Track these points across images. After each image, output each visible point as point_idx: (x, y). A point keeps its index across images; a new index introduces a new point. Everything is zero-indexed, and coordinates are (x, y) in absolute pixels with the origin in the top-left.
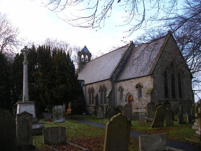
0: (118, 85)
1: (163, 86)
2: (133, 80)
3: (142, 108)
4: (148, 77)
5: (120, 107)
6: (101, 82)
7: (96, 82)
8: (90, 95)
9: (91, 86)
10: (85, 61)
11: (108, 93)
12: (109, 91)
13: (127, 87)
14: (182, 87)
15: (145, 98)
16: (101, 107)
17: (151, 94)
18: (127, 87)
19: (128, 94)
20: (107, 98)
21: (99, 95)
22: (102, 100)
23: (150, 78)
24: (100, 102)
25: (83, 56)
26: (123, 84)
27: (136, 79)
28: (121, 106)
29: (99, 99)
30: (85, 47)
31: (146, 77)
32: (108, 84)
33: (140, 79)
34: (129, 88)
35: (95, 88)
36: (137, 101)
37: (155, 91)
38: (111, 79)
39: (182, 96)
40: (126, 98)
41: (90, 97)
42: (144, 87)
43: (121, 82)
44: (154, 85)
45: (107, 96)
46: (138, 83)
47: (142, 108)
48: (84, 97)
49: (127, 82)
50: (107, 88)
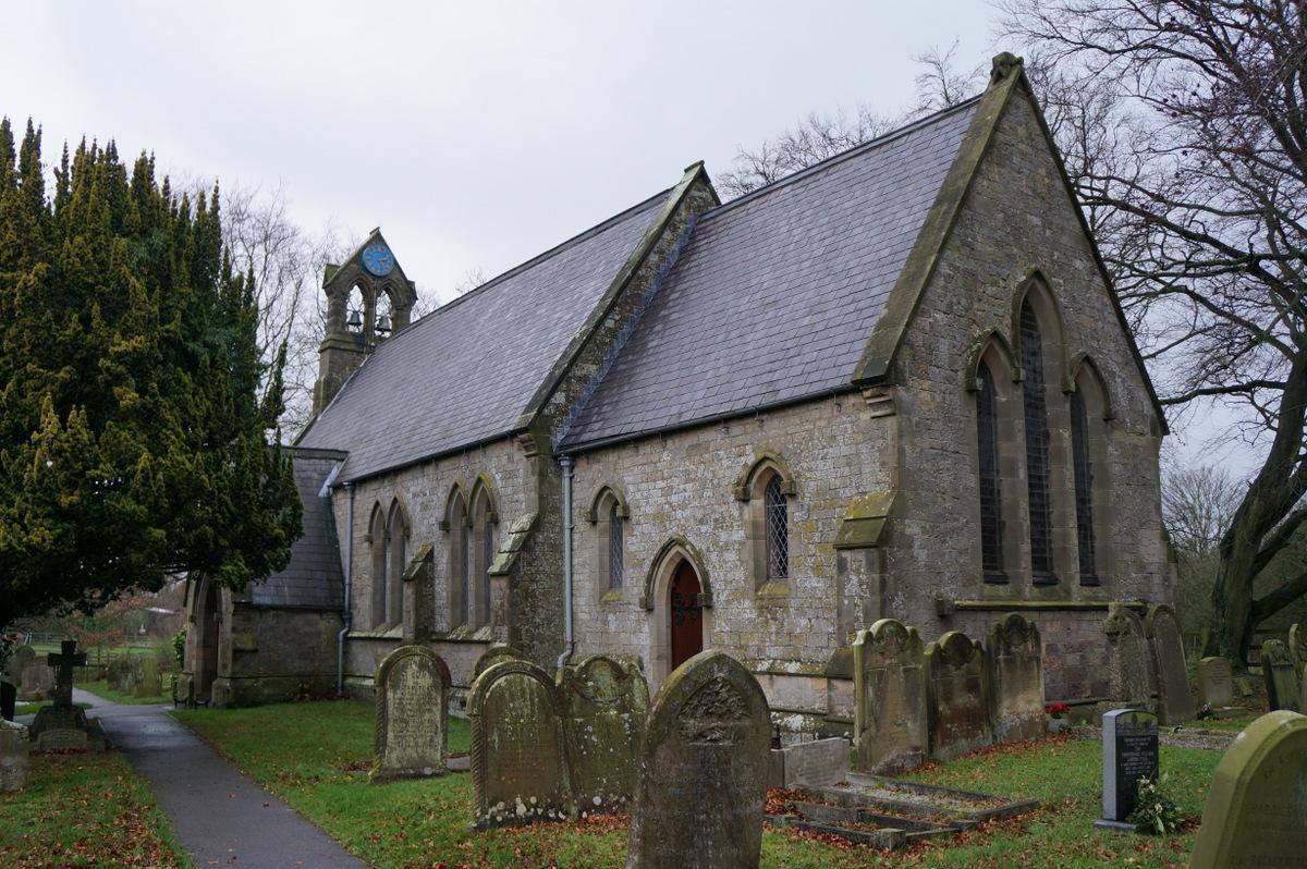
0: (585, 482)
1: (972, 481)
2: (712, 436)
3: (793, 667)
4: (852, 400)
5: (605, 679)
6: (462, 461)
7: (424, 463)
8: (380, 558)
9: (384, 494)
10: (369, 327)
11: (506, 541)
12: (515, 527)
13: (657, 497)
14: (1095, 503)
15: (817, 584)
16: (422, 666)
17: (875, 554)
18: (657, 497)
19: (665, 549)
20: (494, 583)
21: (443, 561)
22: (464, 601)
23: (866, 416)
24: (447, 612)
25: (356, 298)
26: (633, 476)
27: (736, 429)
28: (615, 667)
29: (442, 588)
30: (377, 238)
31: (826, 409)
32: (509, 476)
33: (775, 427)
34: (674, 499)
35: (413, 508)
36: (747, 610)
37: (912, 528)
38: (531, 434)
39: (1100, 573)
40: (650, 579)
41: (380, 576)
42: (809, 489)
43: (612, 457)
44: (904, 479)
45: (499, 562)
46: (751, 459)
47: (793, 667)
48: (341, 572)
49: (664, 456)
50: (504, 509)
